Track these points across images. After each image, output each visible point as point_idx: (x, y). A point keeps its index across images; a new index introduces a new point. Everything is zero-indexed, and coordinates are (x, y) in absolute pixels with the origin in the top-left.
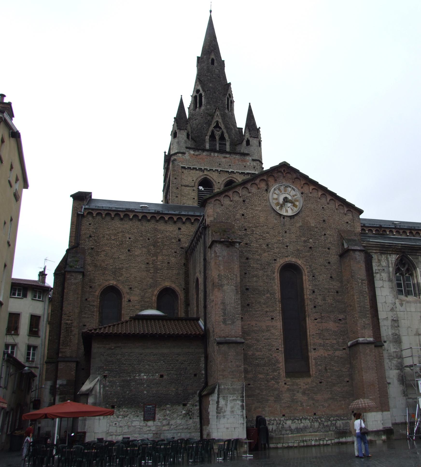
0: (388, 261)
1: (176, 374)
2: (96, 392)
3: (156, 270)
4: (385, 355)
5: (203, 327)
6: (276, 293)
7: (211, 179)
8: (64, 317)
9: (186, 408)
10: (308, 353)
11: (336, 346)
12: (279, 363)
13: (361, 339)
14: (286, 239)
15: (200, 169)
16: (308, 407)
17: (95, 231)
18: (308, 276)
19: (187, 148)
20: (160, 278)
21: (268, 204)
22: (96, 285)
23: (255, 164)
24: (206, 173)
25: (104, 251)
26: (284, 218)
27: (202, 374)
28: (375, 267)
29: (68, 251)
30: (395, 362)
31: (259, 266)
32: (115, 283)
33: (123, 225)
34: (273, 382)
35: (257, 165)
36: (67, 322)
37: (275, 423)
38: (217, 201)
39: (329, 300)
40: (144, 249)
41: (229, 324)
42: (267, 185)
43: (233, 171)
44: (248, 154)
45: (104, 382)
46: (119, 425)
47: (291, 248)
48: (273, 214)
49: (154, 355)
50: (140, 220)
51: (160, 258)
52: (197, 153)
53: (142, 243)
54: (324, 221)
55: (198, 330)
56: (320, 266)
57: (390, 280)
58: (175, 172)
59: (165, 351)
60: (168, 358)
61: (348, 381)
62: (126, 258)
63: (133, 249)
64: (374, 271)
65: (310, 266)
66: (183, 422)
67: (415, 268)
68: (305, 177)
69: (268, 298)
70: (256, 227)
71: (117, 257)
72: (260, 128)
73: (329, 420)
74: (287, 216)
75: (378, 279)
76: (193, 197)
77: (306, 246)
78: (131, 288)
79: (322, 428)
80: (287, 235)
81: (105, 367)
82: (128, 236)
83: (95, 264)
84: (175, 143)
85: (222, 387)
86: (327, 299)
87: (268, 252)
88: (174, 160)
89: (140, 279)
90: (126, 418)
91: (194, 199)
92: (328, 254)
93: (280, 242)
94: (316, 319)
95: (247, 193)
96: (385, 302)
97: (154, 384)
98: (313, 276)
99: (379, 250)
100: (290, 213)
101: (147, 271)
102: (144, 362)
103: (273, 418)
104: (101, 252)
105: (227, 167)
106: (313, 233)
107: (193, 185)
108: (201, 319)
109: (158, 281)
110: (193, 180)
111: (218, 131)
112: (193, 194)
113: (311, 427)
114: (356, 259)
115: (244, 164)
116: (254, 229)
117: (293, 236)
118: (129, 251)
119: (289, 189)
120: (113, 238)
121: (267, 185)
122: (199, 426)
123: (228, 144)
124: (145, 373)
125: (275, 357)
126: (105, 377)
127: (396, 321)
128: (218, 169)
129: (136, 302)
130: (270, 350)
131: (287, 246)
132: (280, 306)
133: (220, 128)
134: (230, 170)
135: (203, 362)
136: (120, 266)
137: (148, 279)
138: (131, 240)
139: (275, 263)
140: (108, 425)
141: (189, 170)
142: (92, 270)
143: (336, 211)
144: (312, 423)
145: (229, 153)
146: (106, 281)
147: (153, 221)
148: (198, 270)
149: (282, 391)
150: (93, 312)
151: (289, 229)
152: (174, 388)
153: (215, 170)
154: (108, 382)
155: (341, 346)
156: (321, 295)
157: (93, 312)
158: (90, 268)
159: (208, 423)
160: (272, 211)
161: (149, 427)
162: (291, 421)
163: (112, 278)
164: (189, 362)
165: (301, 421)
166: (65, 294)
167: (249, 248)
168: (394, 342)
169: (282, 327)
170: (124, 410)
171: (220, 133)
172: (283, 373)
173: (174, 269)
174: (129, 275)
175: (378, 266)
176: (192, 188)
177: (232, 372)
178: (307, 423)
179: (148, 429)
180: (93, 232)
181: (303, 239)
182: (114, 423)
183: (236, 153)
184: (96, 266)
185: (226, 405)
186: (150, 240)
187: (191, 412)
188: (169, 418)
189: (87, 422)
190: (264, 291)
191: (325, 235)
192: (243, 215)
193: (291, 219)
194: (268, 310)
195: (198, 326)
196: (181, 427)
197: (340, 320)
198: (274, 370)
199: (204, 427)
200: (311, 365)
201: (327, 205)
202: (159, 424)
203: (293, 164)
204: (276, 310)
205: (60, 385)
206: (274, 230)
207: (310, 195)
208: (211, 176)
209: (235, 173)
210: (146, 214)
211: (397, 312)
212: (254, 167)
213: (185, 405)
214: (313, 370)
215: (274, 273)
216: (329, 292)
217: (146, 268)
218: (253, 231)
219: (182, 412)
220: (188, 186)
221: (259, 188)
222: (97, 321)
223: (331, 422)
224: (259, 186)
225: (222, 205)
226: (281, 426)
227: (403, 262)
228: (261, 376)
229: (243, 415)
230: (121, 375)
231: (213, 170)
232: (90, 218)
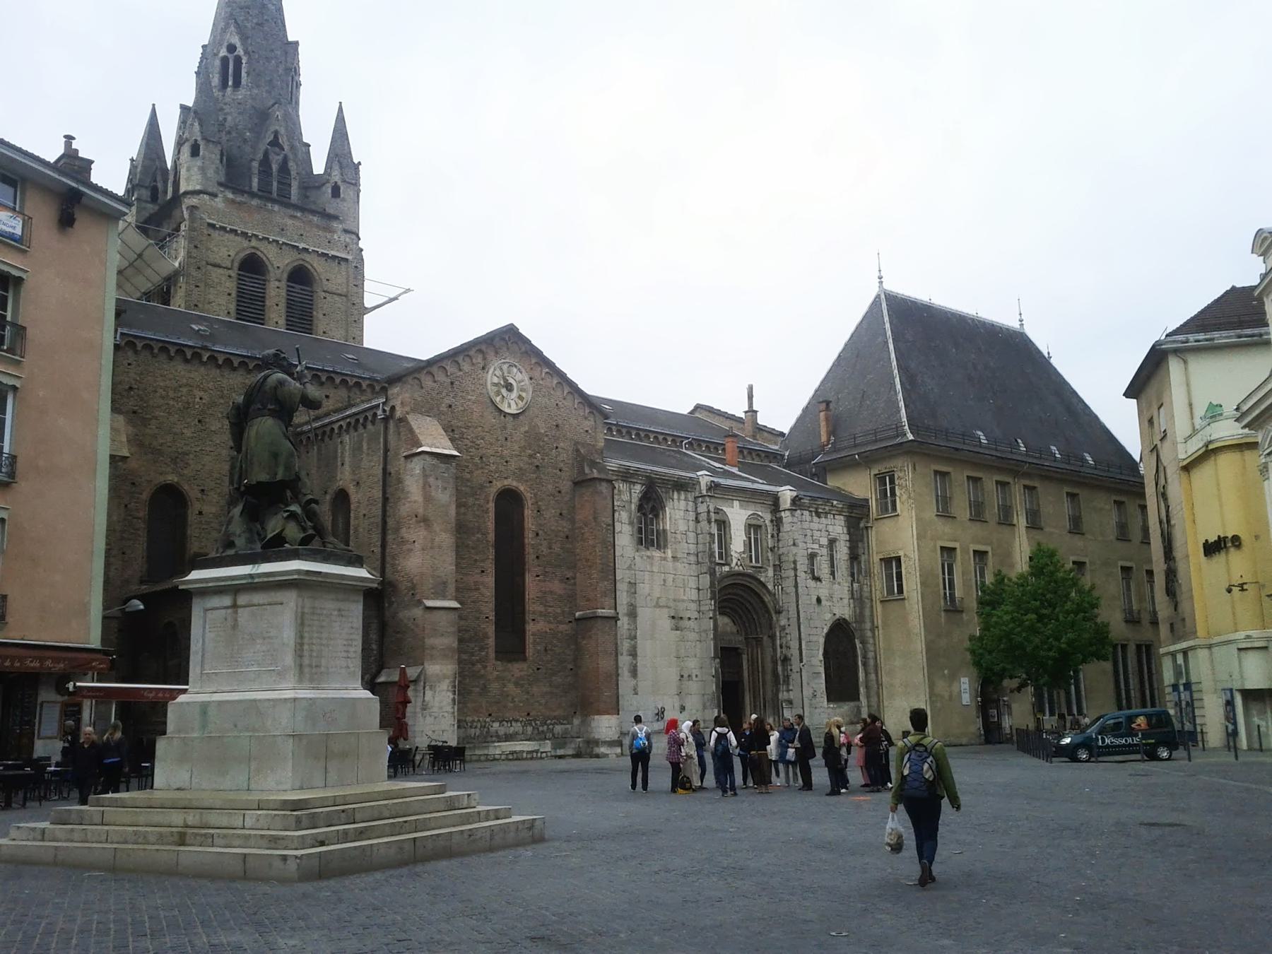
6: (488, 533)
10: (524, 625)
11: (560, 618)
12: (488, 638)
13: (600, 612)
15: (244, 234)
19: (220, 184)
21: (484, 391)
23: (347, 240)
24: (254, 243)
25: (156, 418)
26: (505, 416)
27: (372, 650)
31: (468, 490)
32: (176, 480)
33: (190, 372)
37: (479, 725)
39: (557, 548)
42: (485, 359)
43: (307, 247)
44: (336, 218)
48: (491, 409)
50: (219, 367)
52: (239, 199)
54: (557, 426)
57: (631, 523)
58: (195, 233)
62: (195, 435)
63: (207, 420)
65: (535, 495)
67: (663, 508)
68: (537, 353)
69: (478, 540)
70: (468, 428)
71: (178, 431)
72: (359, 163)
73: (545, 724)
74: (509, 414)
76: (228, 291)
78: (203, 490)
82: (198, 394)
84: (196, 169)
89: (219, 475)
91: (229, 294)
93: (498, 454)
94: (538, 576)
99: (622, 476)
100: (513, 410)
104: (151, 419)
105: (296, 237)
106: (541, 444)
107: (230, 267)
110: (229, 256)
111: (278, 155)
112: (228, 284)
114: (602, 493)
116: (463, 430)
118: (199, 421)
120: (171, 394)
121: (485, 359)
129: (211, 515)
134: (301, 246)
136: (186, 448)
138: (204, 401)
139: (490, 487)
141: (222, 233)
143: (573, 411)
145: (295, 207)
147: (241, 371)
149: (489, 680)
150: (138, 530)
153: (274, 241)
157: (138, 530)
160: (490, 404)
171: (280, 158)
172: (492, 655)
174: (200, 467)
178: (517, 727)
192: (450, 406)
193: (514, 418)
197: (568, 579)
198: (482, 649)
200: (527, 642)
201: (563, 401)
203: (1124, 392)
207: (541, 382)
208: (265, 252)
209: (309, 253)
210: (246, 360)
211: (635, 570)
214: (530, 651)
215: (488, 503)
216: (556, 536)
218: (462, 433)
220: (219, 266)
221: (473, 364)
223: (548, 726)
224: (474, 360)
225: (422, 388)
226: (486, 730)
229: (454, 713)
231: (268, 239)
232: (130, 353)
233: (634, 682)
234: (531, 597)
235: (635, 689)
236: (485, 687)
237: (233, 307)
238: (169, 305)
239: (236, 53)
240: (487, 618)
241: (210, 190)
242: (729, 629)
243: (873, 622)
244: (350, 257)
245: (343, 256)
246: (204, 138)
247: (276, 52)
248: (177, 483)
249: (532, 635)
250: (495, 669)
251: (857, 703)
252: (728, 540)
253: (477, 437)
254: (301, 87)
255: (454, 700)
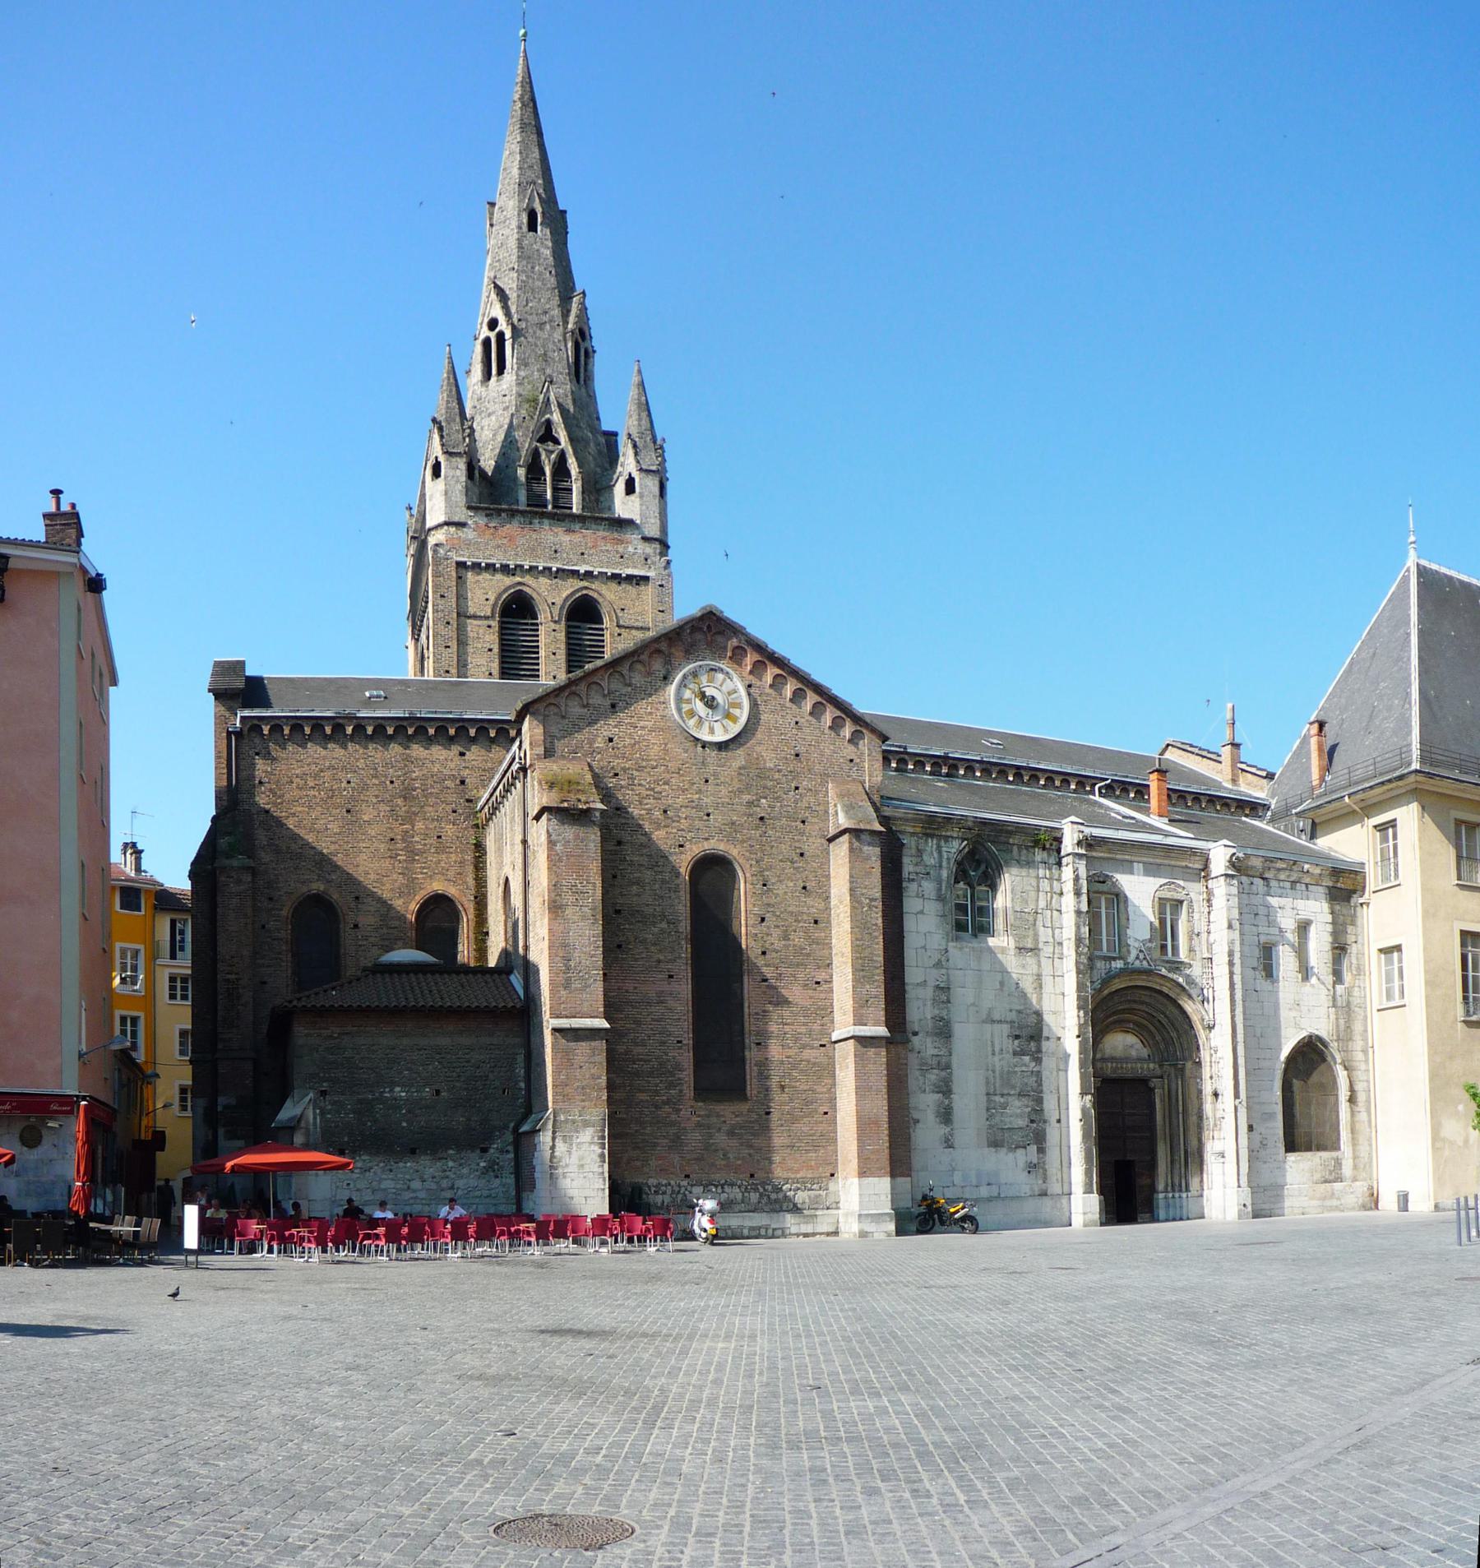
0: (940, 853)
1: (465, 1089)
2: (307, 1122)
3: (412, 853)
4: (913, 1061)
5: (521, 993)
7: (534, 595)
8: (221, 967)
9: (488, 1156)
14: (707, 797)
15: (505, 569)
16: (739, 1162)
17: (269, 769)
18: (752, 884)
20: (422, 873)
22: (282, 893)
25: (294, 815)
26: (703, 747)
27: (520, 1089)
28: (908, 866)
29: (214, 820)
30: (933, 1076)
31: (644, 860)
32: (322, 889)
34: (667, 1109)
35: (655, 553)
36: (229, 976)
37: (669, 1192)
38: (552, 707)
40: (384, 808)
41: (576, 989)
43: (591, 569)
45: (322, 1104)
46: (355, 1186)
47: (717, 819)
49: (420, 1050)
51: (419, 825)
53: (376, 793)
55: (511, 997)
56: (781, 861)
57: (940, 898)
58: (441, 579)
59: (444, 1041)
60: (449, 1056)
61: (826, 1113)
64: (905, 875)
66: (482, 1183)
69: (662, 931)
70: (640, 769)
75: (914, 894)
76: (488, 646)
77: (752, 815)
78: (357, 898)
79: (766, 1204)
80: (710, 787)
81: (322, 1075)
83: (277, 846)
85: (562, 1118)
86: (791, 937)
87: (665, 826)
88: (436, 545)
90: (368, 1173)
91: (490, 650)
92: (802, 834)
93: (694, 804)
95: (620, 686)
96: (924, 947)
97: (421, 1109)
98: (764, 885)
100: (719, 737)
101: (391, 857)
102: (399, 1063)
103: (664, 1182)
105: (575, 558)
107: (489, 614)
108: (515, 971)
109: (416, 881)
113: (743, 1202)
115: (621, 549)
117: (724, 791)
118: (348, 811)
119: (720, 676)
122: (514, 1193)
123: (576, 487)
124: (403, 1086)
125: (674, 1057)
126: (324, 1093)
127: (944, 991)
128: (550, 565)
129: (369, 928)
130: (663, 1043)
131: (708, 815)
132: (689, 950)
133: (557, 442)
134: (582, 569)
135: (522, 1065)
137: (395, 876)
138: (352, 784)
140: (334, 1185)
142: (272, 861)
144: (746, 1194)
145: (580, 519)
146: (303, 883)
148: (507, 859)
149: (685, 1128)
150: (280, 953)
151: (715, 774)
152: (462, 1116)
154: (330, 1103)
155: (816, 1039)
156: (778, 927)
158: (265, 857)
159: (533, 1187)
161: (414, 1191)
162: (702, 1187)
163: (316, 877)
164: (493, 1065)
165: (722, 1188)
166: (218, 917)
167: (625, 817)
168: (936, 1034)
169: (690, 995)
170: (363, 1157)
172: (689, 1092)
173: (451, 850)
175: (916, 865)
176: (486, 623)
177: (583, 1088)
179: (412, 1195)
180: (266, 772)
181: (746, 797)
182: (346, 1182)
183: (598, 520)
184: (278, 851)
185: (569, 1152)
186: (396, 785)
187: (498, 1164)
188: (453, 1176)
189: (294, 1181)
190: (654, 916)
191: (797, 788)
192: (611, 740)
194: (662, 958)
195: (512, 992)
196: (478, 1193)
197: (818, 983)
198: (671, 1085)
199: (524, 1195)
202: (434, 1186)
204: (680, 958)
205: (226, 1107)
206: (682, 775)
212: (646, 560)
213: (484, 1150)
217: (389, 849)
218: (632, 778)
219: (478, 1165)
222: (289, 971)
226: (680, 1197)
227: (977, 857)
228: (643, 1096)
230: (354, 1089)
232: (257, 741)
233: (945, 1130)
234: (753, 1011)
235: (947, 1140)
236: (679, 1138)
237: (495, 667)
238: (467, 677)
239: (497, 330)
240: (679, 1042)
241: (456, 519)
242: (1134, 1053)
243: (1365, 1040)
244: (651, 574)
245: (642, 573)
246: (446, 453)
247: (552, 313)
248: (323, 892)
249: (755, 1065)
250: (693, 1113)
251: (1334, 1154)
252: (1123, 921)
253: (656, 782)
254: (596, 356)
255: (602, 1155)
